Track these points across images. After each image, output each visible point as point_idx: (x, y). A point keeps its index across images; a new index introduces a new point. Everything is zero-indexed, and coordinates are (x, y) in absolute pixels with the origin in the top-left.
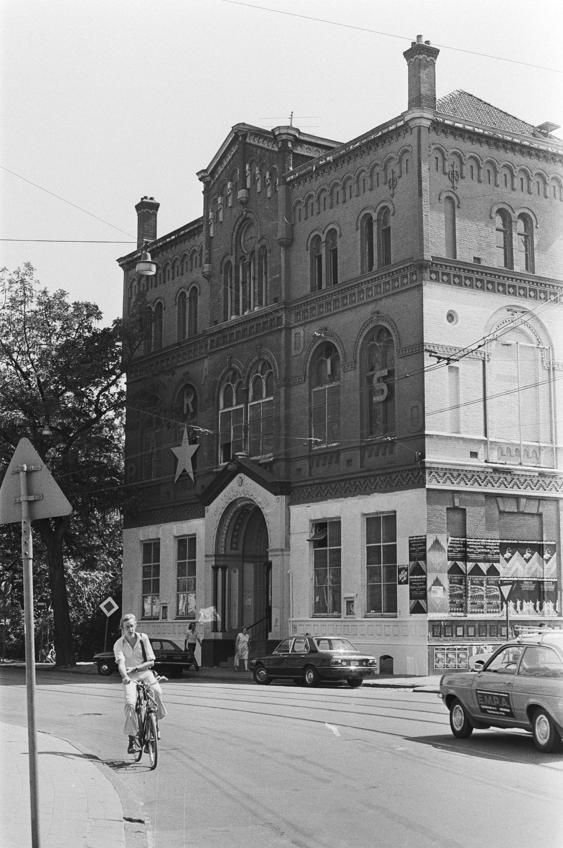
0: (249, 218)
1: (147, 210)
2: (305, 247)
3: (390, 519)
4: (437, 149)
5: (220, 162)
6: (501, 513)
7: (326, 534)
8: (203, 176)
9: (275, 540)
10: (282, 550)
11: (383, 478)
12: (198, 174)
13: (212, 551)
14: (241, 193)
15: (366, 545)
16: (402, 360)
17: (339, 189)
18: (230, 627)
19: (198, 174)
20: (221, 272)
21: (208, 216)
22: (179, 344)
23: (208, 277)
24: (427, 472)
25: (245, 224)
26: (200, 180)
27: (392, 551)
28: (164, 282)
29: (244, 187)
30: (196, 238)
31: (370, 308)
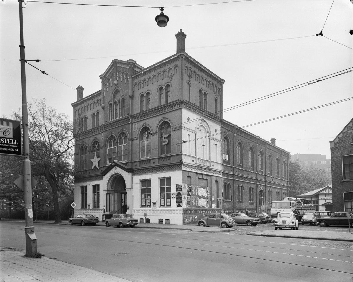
0: (118, 90)
1: (80, 90)
2: (138, 98)
3: (169, 179)
4: (186, 66)
5: (107, 73)
6: (199, 178)
7: (146, 184)
8: (102, 77)
9: (128, 186)
10: (131, 189)
11: (166, 167)
12: (71, 104)
13: (106, 189)
14: (115, 82)
15: (159, 187)
16: (174, 132)
17: (151, 79)
18: (111, 211)
19: (100, 76)
20: (108, 107)
21: (103, 89)
22: (93, 129)
23: (103, 108)
24: (183, 165)
25: (117, 92)
26: (101, 78)
27: (169, 189)
28: (87, 111)
29: (116, 80)
30: (99, 97)
31: (162, 116)
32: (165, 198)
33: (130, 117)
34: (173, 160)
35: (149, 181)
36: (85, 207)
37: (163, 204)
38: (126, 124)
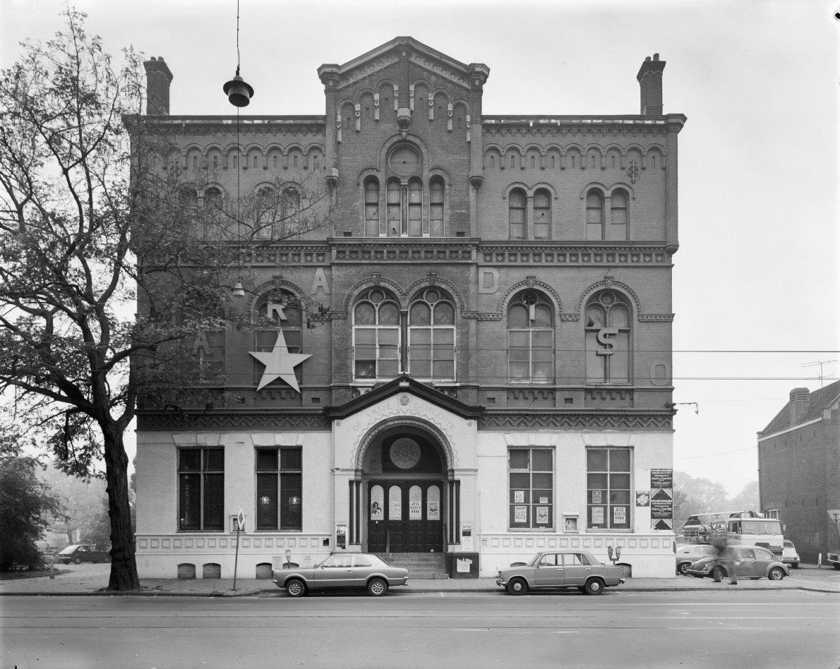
5: (360, 68)
16: (644, 327)
32: (609, 505)
33: (473, 245)
34: (642, 403)
35: (546, 454)
36: (202, 527)
37: (521, 517)
38: (452, 264)
